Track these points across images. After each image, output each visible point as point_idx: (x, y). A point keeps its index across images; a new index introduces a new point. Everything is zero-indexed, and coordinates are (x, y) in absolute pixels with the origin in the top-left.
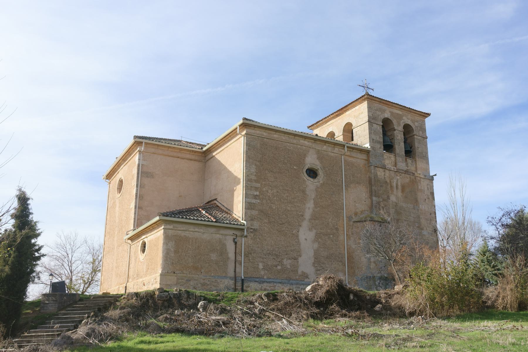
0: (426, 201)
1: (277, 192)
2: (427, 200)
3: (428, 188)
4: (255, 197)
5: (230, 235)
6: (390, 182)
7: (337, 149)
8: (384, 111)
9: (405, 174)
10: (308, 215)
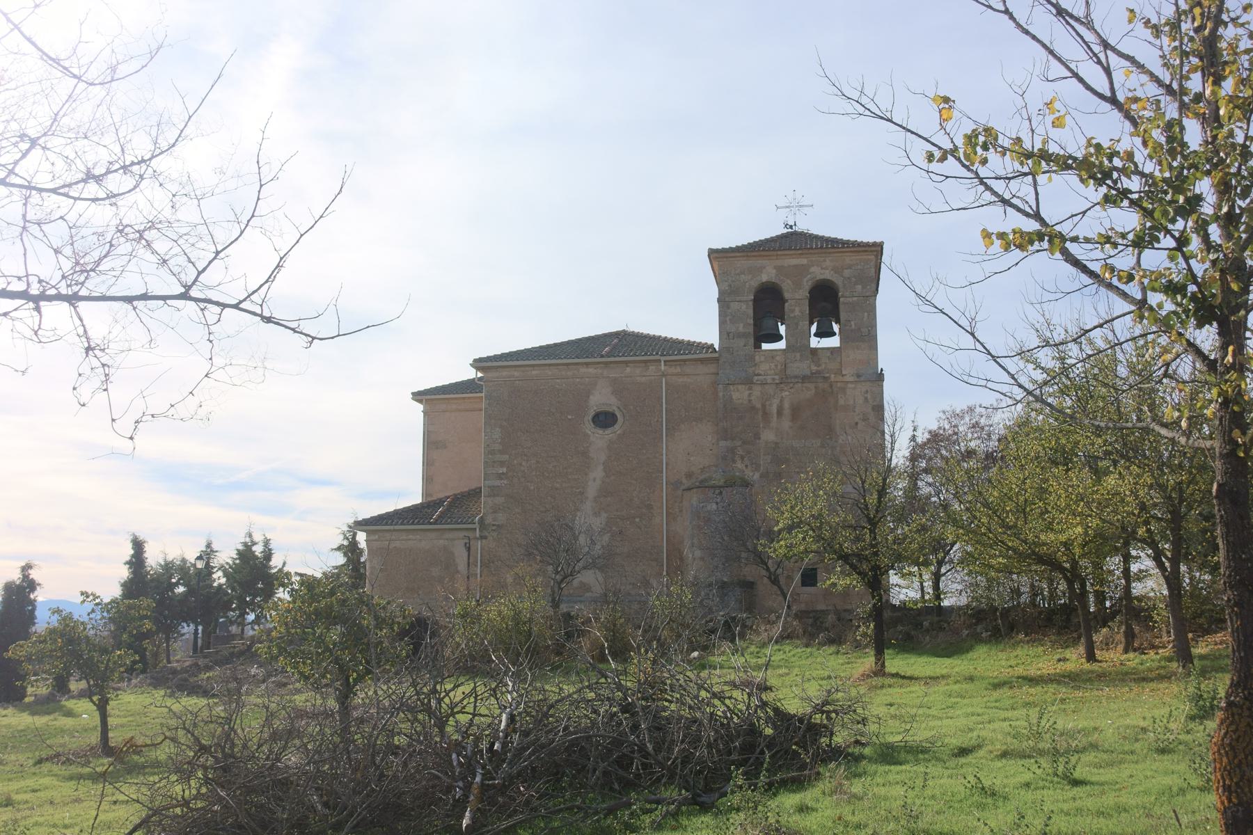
0: (859, 425)
1: (538, 462)
2: (861, 425)
3: (866, 398)
4: (500, 476)
5: (459, 539)
6: (764, 406)
7: (654, 367)
8: (761, 269)
9: (802, 383)
10: (592, 490)
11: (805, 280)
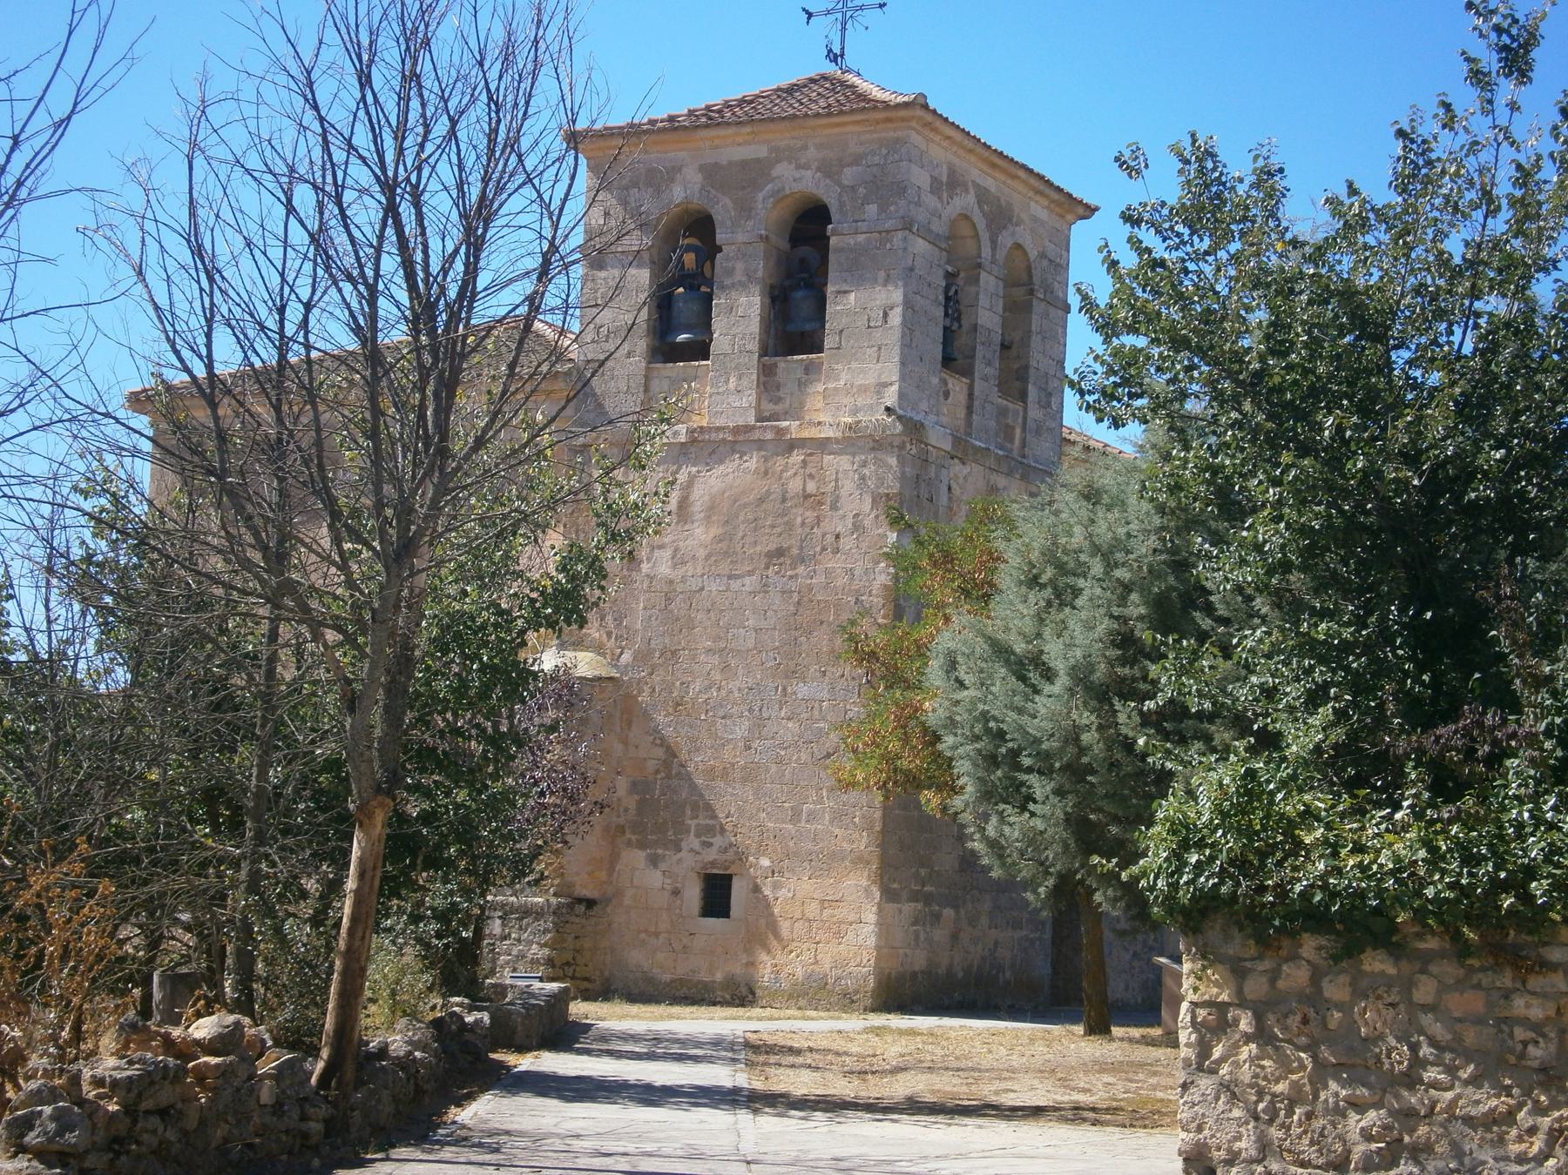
11: (760, 196)
